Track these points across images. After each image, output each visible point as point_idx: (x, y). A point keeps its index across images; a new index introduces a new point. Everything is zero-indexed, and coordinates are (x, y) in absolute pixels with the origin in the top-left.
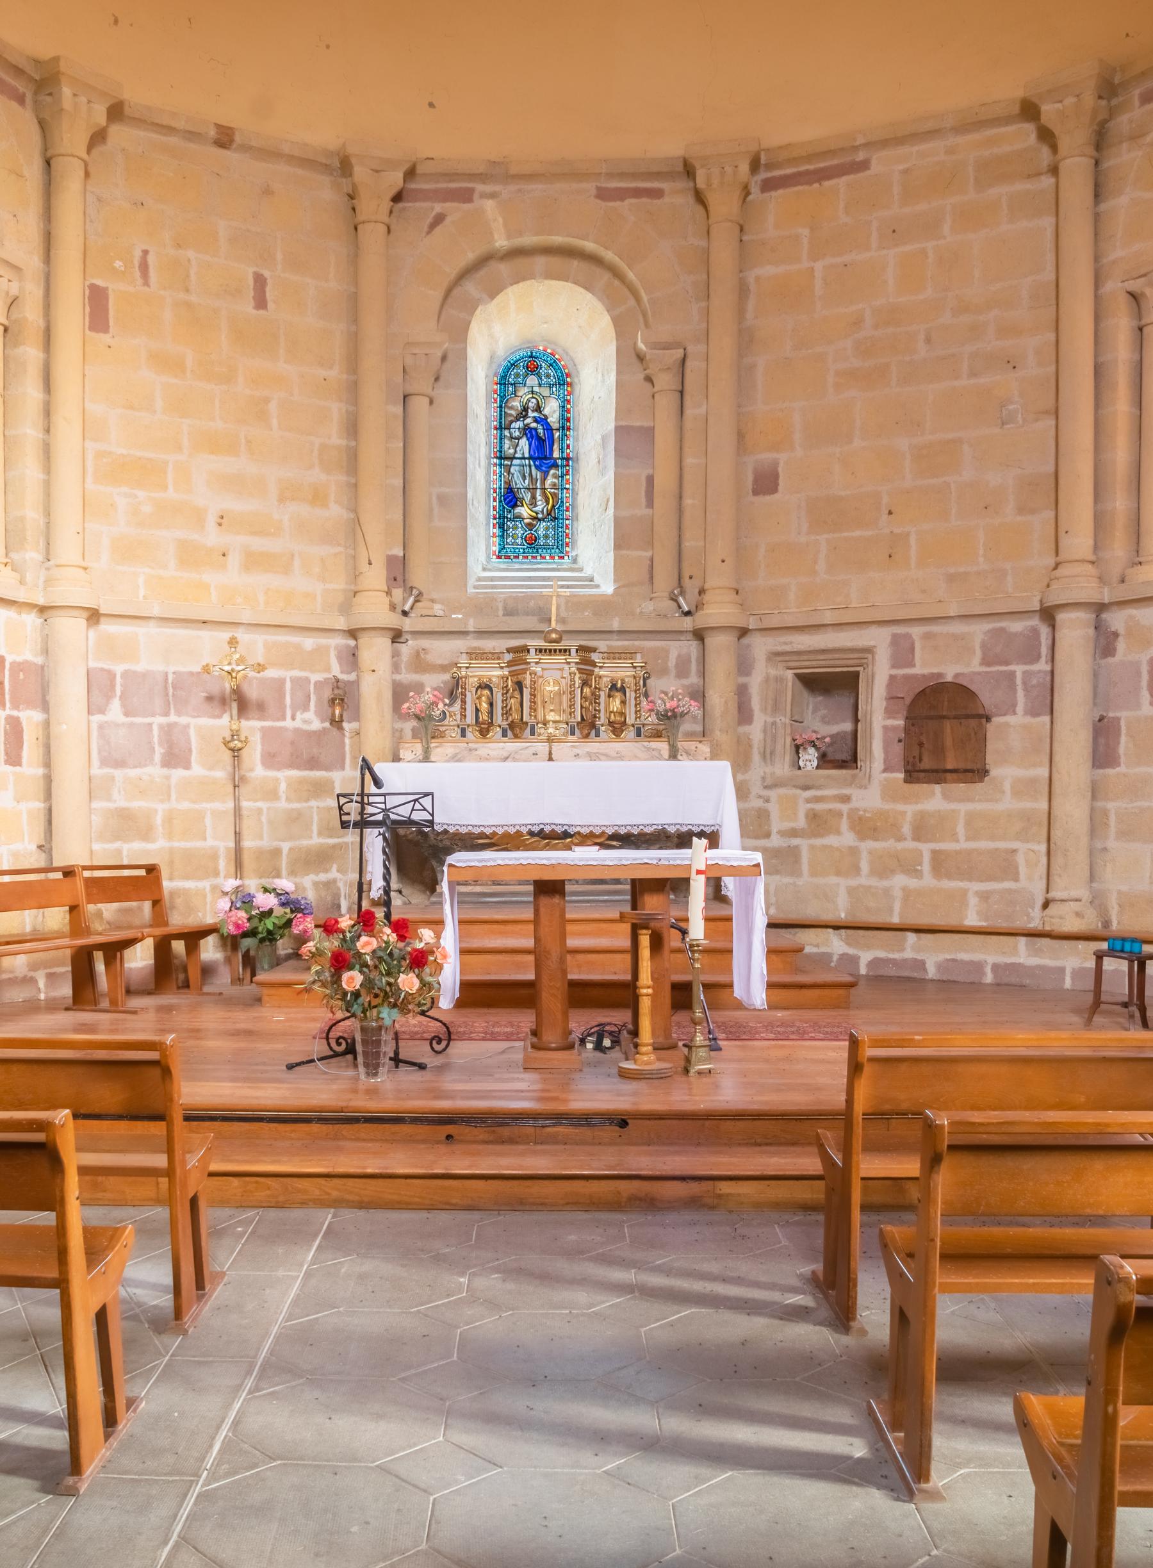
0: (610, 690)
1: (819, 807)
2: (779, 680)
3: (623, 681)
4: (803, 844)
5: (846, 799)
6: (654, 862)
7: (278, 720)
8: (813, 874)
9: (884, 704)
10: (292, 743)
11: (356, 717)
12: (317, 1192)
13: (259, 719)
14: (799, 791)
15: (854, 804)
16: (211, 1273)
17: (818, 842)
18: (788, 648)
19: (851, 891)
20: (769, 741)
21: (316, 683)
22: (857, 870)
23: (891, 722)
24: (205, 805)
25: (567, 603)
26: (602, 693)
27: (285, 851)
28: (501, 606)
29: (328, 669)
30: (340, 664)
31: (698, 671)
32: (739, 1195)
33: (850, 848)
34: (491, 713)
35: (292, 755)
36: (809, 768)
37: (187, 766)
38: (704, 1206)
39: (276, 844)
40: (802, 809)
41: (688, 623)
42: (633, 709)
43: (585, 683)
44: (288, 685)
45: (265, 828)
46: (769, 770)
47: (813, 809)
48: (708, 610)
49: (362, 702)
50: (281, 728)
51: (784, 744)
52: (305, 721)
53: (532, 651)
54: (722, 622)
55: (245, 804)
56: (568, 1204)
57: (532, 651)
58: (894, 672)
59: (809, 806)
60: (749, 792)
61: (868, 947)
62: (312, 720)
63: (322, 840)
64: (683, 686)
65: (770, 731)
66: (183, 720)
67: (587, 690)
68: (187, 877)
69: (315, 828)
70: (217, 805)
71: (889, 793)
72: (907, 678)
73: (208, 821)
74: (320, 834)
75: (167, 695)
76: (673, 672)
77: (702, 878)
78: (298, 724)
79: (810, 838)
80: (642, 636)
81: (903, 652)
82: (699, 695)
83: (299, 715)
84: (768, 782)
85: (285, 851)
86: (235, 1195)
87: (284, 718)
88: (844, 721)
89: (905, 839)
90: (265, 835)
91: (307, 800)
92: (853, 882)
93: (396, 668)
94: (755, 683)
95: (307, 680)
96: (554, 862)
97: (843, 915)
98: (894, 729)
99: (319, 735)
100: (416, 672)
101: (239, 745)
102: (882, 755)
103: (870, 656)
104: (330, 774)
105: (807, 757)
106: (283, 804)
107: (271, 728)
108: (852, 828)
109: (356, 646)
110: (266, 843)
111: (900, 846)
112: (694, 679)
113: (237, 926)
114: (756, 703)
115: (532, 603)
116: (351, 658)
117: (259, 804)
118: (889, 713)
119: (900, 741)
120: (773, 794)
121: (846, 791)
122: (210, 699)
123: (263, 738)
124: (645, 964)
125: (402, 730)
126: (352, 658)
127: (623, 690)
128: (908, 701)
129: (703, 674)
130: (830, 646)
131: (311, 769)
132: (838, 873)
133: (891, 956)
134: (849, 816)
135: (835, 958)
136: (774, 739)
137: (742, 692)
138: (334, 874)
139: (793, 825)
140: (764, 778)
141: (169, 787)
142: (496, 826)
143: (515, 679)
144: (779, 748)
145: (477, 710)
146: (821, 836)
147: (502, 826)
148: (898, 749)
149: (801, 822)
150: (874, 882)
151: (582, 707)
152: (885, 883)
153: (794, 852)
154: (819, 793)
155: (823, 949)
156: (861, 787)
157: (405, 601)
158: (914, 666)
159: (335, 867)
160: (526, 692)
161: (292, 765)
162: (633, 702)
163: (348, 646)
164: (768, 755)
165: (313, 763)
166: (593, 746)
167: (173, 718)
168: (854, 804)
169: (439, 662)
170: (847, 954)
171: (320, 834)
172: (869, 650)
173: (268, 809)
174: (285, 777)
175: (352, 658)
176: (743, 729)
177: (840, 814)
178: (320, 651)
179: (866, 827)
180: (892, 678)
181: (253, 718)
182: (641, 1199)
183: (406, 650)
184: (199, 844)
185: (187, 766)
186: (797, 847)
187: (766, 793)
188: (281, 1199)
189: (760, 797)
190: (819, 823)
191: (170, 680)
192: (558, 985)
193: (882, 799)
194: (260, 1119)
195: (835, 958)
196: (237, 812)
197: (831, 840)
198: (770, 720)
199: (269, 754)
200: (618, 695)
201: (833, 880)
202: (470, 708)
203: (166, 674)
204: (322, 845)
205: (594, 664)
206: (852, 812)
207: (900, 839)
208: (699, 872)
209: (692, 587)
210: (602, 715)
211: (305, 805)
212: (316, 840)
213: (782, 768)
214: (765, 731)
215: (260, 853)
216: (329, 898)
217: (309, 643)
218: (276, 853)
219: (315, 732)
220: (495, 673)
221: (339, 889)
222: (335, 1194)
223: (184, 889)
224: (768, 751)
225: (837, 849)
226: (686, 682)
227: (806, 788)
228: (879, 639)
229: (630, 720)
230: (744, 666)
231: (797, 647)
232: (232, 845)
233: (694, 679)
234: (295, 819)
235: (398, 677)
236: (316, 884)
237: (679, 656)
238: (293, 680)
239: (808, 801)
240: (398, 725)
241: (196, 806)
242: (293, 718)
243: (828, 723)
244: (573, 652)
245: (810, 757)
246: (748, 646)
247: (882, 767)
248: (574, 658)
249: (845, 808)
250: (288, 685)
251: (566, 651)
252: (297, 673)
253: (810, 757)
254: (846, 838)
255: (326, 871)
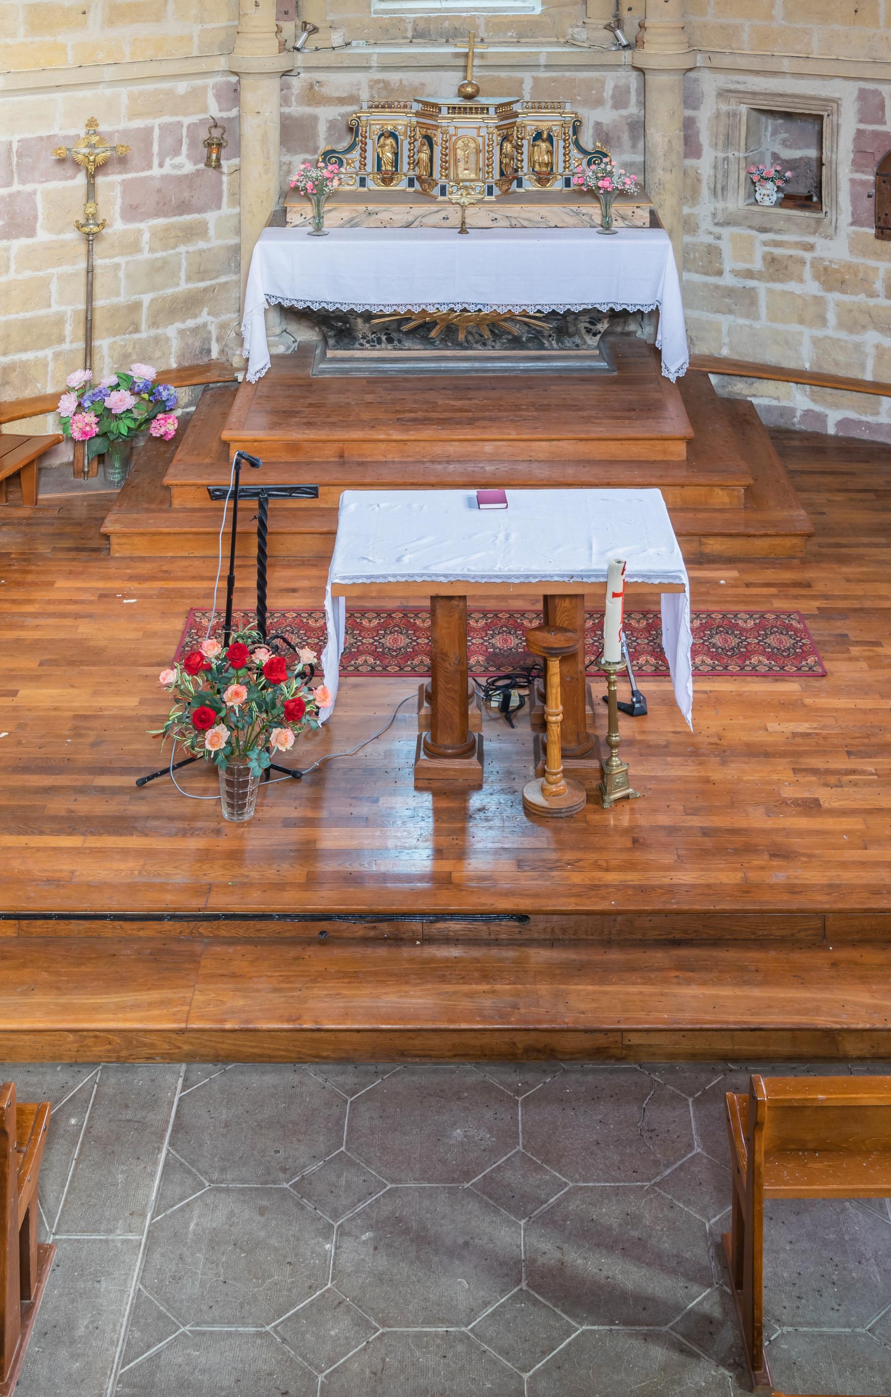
0: (535, 139)
1: (777, 251)
2: (733, 115)
3: (550, 130)
4: (761, 287)
5: (810, 247)
6: (566, 579)
7: (143, 170)
8: (772, 318)
9: (852, 156)
10: (159, 191)
11: (237, 153)
12: (166, 1046)
13: (120, 173)
14: (754, 233)
15: (818, 253)
16: (40, 1247)
17: (778, 286)
18: (741, 87)
19: (815, 341)
20: (720, 176)
21: (189, 126)
22: (822, 320)
23: (858, 176)
24: (50, 271)
25: (487, 24)
26: (525, 142)
27: (146, 304)
28: (410, 27)
29: (205, 109)
30: (219, 103)
31: (638, 102)
32: (651, 1046)
33: (815, 297)
34: (396, 163)
35: (158, 203)
36: (767, 203)
37: (32, 233)
38: (610, 1057)
39: (134, 298)
40: (759, 252)
41: (626, 56)
42: (561, 158)
43: (505, 138)
44: (156, 133)
45: (123, 283)
46: (720, 205)
47: (771, 253)
48: (649, 49)
49: (244, 143)
50: (146, 178)
51: (738, 176)
52: (175, 167)
53: (444, 110)
54: (665, 64)
55: (98, 262)
56: (455, 1056)
57: (444, 110)
58: (862, 126)
59: (767, 249)
60: (697, 226)
61: (836, 406)
62: (184, 164)
63: (191, 286)
64: (621, 116)
65: (722, 167)
66: (28, 188)
67: (508, 147)
68: (25, 349)
69: (183, 275)
70: (67, 269)
71: (855, 245)
72: (876, 134)
73: (54, 287)
74: (189, 279)
75: (11, 164)
76: (609, 103)
77: (620, 600)
78: (167, 170)
79: (768, 281)
80: (572, 68)
81: (872, 107)
82: (638, 128)
83: (168, 161)
84: (720, 218)
85: (146, 304)
86: (70, 1050)
87: (150, 167)
88: (808, 147)
89: (878, 296)
90: (122, 291)
91: (176, 246)
92: (819, 333)
93: (285, 101)
94: (704, 117)
95: (180, 124)
96: (453, 579)
97: (807, 366)
98: (863, 183)
99: (190, 179)
100: (309, 105)
101: (95, 229)
102: (850, 209)
103: (835, 105)
104: (204, 215)
105: (765, 192)
106: (146, 255)
107: (133, 180)
108: (817, 277)
109: (239, 82)
110: (122, 299)
111: (872, 302)
112: (633, 109)
113: (85, 433)
114: (705, 138)
115: (446, 24)
116: (232, 95)
117: (117, 260)
118: (857, 165)
119: (869, 196)
120: (726, 232)
121: (811, 239)
122: (61, 161)
123: (124, 192)
124: (554, 691)
125: (290, 163)
126: (233, 95)
127: (550, 139)
128: (879, 157)
129: (643, 104)
130: (790, 91)
131: (181, 214)
132: (801, 322)
133: (864, 418)
134: (813, 265)
135: (799, 414)
136: (726, 174)
137: (689, 127)
138: (204, 317)
139: (748, 266)
140: (714, 215)
141: (8, 258)
142: (398, 305)
143: (424, 131)
144: (732, 182)
145: (379, 159)
146: (782, 281)
147: (405, 305)
148: (869, 204)
149: (758, 265)
150: (843, 335)
151: (501, 163)
152: (856, 338)
153: (750, 296)
154: (778, 237)
155: (784, 403)
156: (826, 237)
157: (296, 38)
158: (885, 123)
159: (206, 310)
160: (437, 150)
161: (157, 214)
162: (561, 151)
163: (228, 83)
164: (719, 191)
165: (183, 208)
166: (515, 210)
167: (16, 187)
168: (818, 253)
169: (337, 94)
170: (812, 411)
171: (189, 279)
172: (836, 101)
173: (127, 263)
174: (147, 227)
175: (233, 95)
176: (689, 162)
177: (803, 262)
178: (196, 94)
179: (832, 278)
180: (860, 132)
181: (113, 173)
182: (539, 1051)
183: (297, 84)
184: (42, 312)
185: (32, 233)
186: (753, 289)
187: (718, 230)
188: (124, 1053)
189: (710, 233)
190: (778, 268)
191: (15, 149)
192: (457, 688)
193: (851, 252)
194: (103, 917)
195: (799, 414)
196: (90, 271)
197: (792, 286)
198: (721, 155)
199: (131, 206)
200: (544, 145)
201: (795, 327)
202: (369, 154)
203: (10, 143)
204: (190, 290)
205: (516, 115)
206: (815, 262)
207: (872, 295)
208: (615, 595)
209: (630, 20)
210: (525, 164)
211: (171, 252)
212: (184, 286)
213: (736, 203)
214: (715, 167)
215: (113, 312)
216: (198, 344)
217: (182, 87)
218: (135, 307)
219: (186, 176)
220: (400, 121)
221: (210, 333)
222: (186, 1047)
223: (21, 361)
224: (719, 186)
225: (799, 296)
226: (625, 112)
227: (763, 230)
228: (846, 94)
229: (559, 167)
230: (691, 99)
231: (750, 87)
232: (82, 306)
233: (633, 109)
234: (160, 269)
235: (286, 110)
236: (181, 332)
237: (616, 87)
238: (161, 127)
239: (765, 244)
240: (286, 158)
241: (41, 273)
242: (161, 165)
243: (790, 147)
244: (492, 110)
245: (768, 193)
246: (696, 80)
247: (850, 220)
248: (493, 120)
249: (808, 256)
250: (156, 133)
251: (484, 109)
252: (167, 119)
253: (768, 192)
254: (812, 287)
255: (195, 316)
